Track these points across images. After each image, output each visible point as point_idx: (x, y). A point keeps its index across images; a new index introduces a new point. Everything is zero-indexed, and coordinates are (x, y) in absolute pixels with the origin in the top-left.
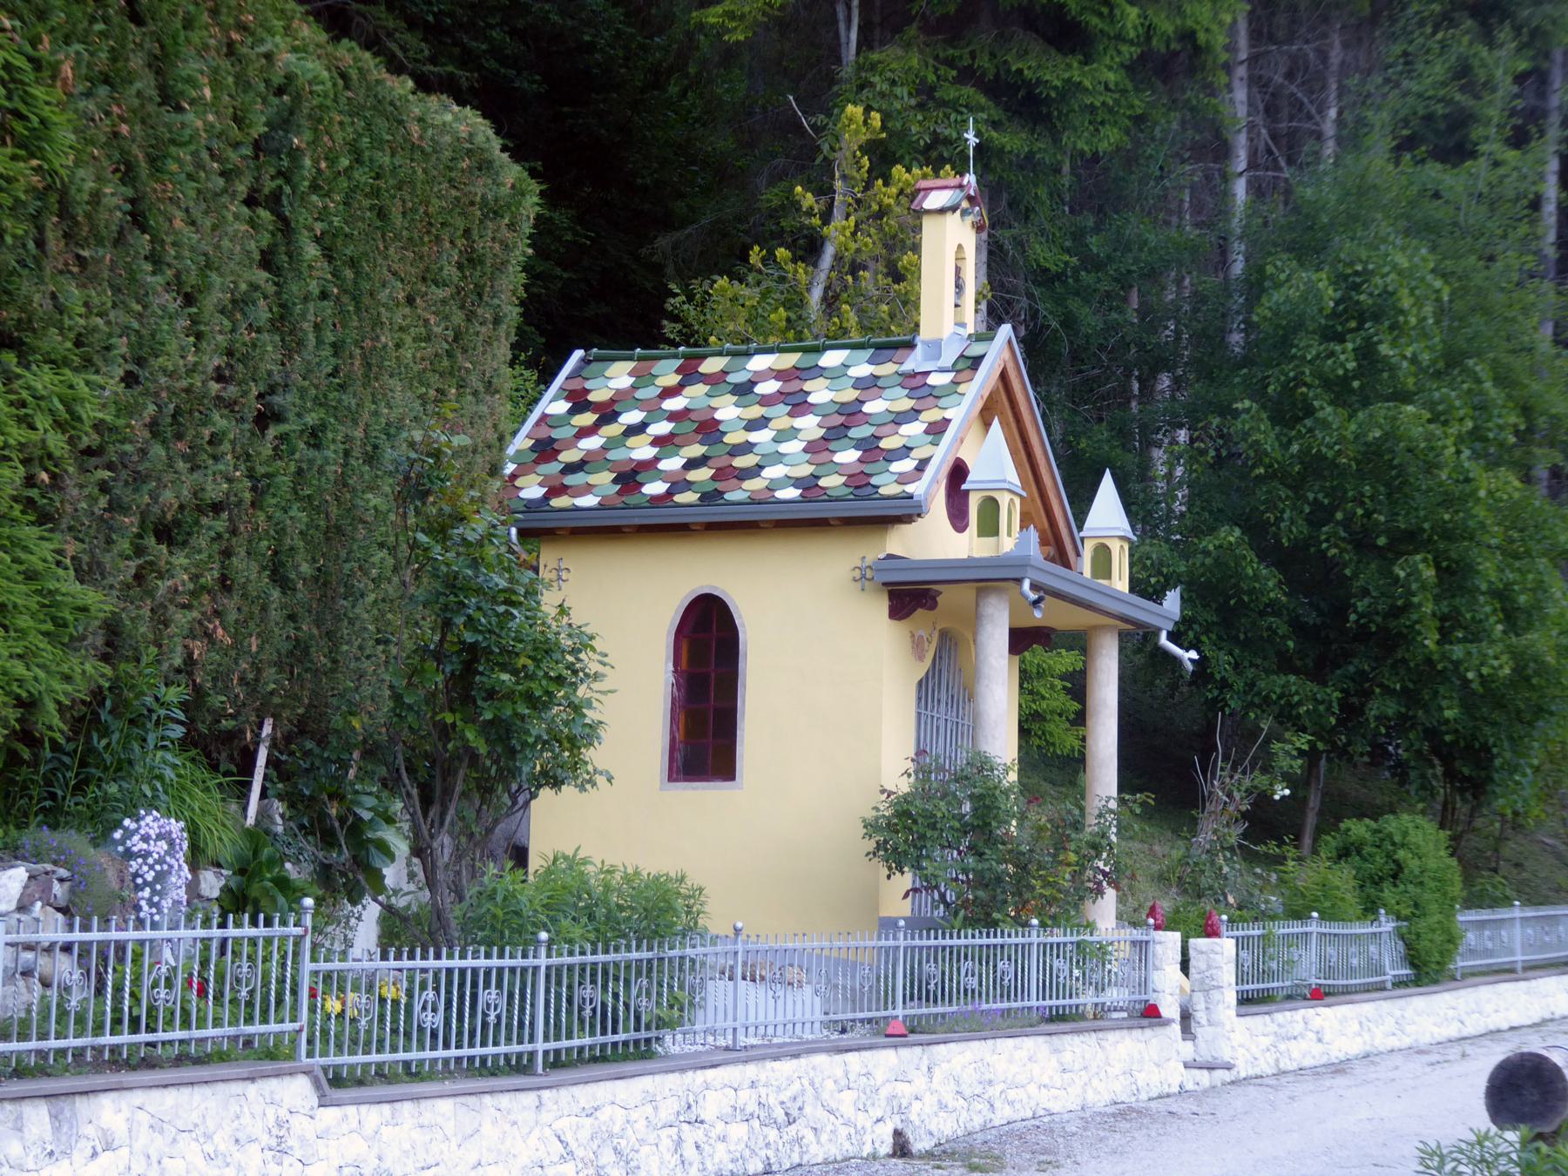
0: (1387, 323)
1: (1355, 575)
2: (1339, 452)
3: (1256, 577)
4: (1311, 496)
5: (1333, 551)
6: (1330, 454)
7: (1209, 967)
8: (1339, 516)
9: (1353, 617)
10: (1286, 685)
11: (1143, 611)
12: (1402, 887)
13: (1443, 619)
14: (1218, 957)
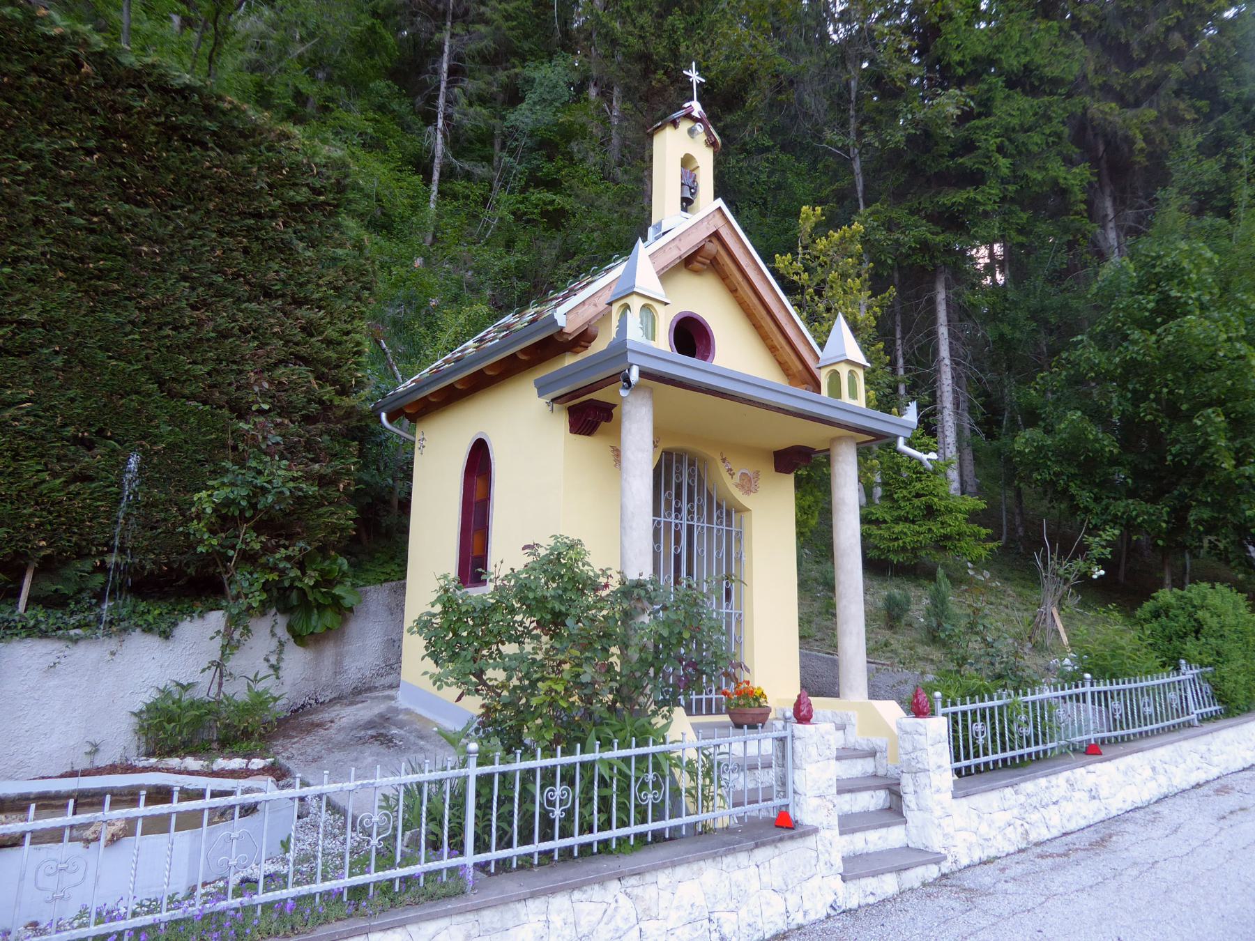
0: (1176, 281)
1: (1169, 432)
2: (1145, 355)
3: (1096, 440)
4: (1130, 387)
5: (1149, 417)
6: (1139, 358)
7: (915, 749)
8: (1152, 396)
9: (1169, 458)
10: (1127, 505)
11: (881, 422)
12: (1203, 640)
13: (1237, 451)
14: (922, 738)
